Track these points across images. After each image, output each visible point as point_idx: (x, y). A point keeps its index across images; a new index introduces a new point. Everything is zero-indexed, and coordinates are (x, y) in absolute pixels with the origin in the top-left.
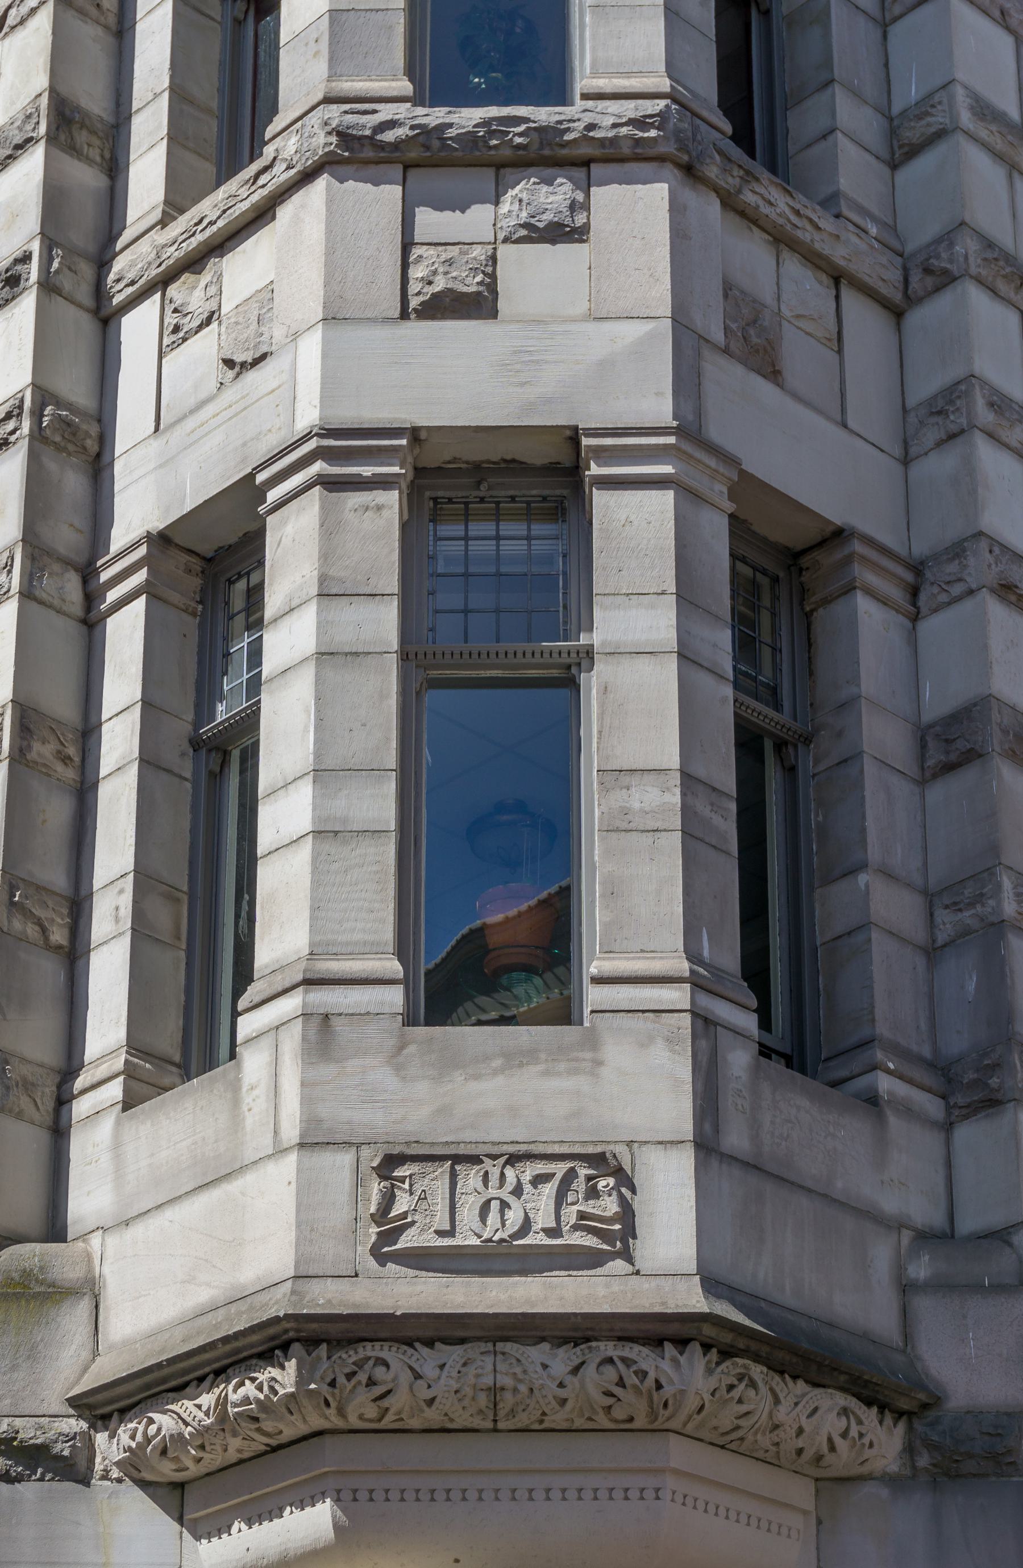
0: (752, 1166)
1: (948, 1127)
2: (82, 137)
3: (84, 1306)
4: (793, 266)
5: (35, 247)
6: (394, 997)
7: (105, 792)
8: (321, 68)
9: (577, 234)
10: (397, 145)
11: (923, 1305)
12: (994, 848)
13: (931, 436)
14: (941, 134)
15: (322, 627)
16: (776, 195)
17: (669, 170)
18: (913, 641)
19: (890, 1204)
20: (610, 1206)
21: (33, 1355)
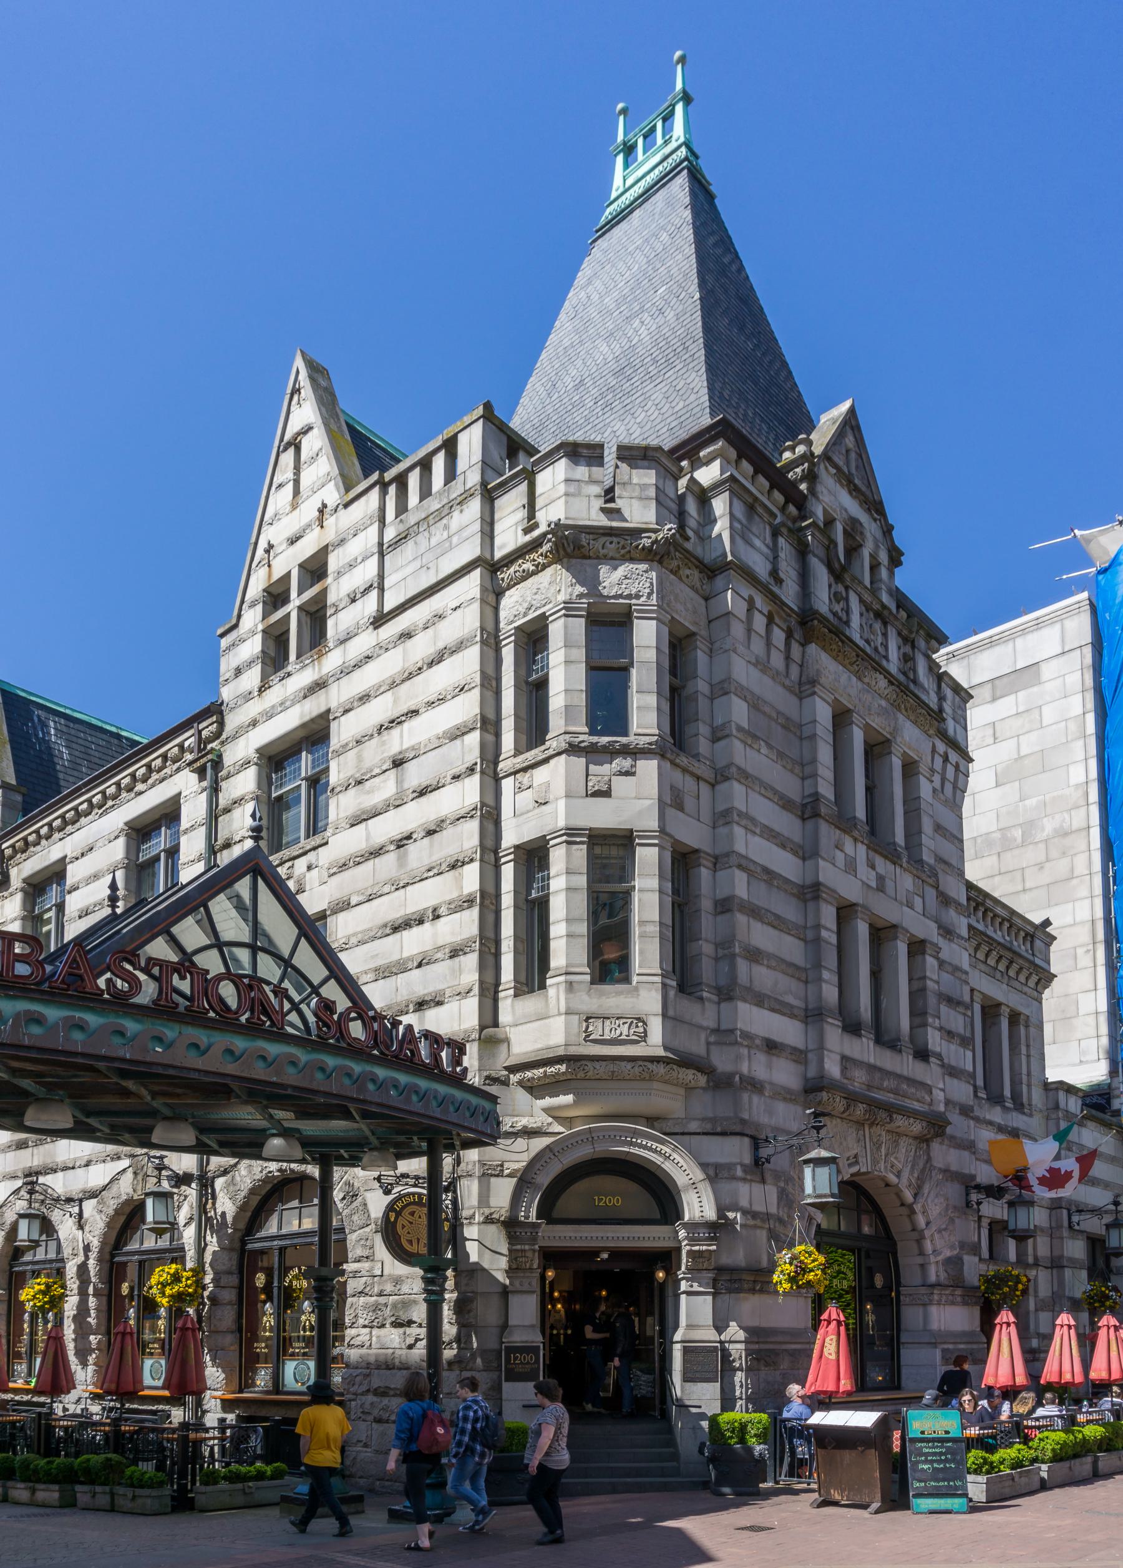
0: (674, 1019)
1: (719, 1003)
2: (489, 727)
3: (506, 1044)
4: (688, 778)
5: (479, 761)
6: (588, 978)
7: (503, 913)
8: (562, 722)
9: (633, 774)
10: (585, 747)
11: (713, 1048)
12: (734, 936)
13: (721, 822)
14: (727, 736)
15: (567, 881)
16: (684, 759)
17: (658, 757)
18: (714, 877)
19: (705, 1024)
20: (642, 1030)
21: (494, 1056)
